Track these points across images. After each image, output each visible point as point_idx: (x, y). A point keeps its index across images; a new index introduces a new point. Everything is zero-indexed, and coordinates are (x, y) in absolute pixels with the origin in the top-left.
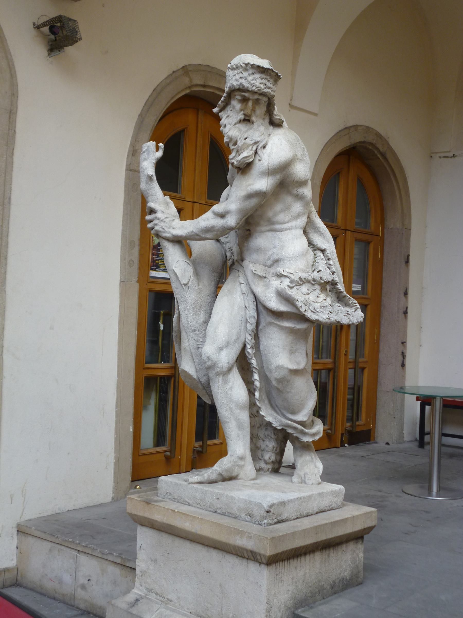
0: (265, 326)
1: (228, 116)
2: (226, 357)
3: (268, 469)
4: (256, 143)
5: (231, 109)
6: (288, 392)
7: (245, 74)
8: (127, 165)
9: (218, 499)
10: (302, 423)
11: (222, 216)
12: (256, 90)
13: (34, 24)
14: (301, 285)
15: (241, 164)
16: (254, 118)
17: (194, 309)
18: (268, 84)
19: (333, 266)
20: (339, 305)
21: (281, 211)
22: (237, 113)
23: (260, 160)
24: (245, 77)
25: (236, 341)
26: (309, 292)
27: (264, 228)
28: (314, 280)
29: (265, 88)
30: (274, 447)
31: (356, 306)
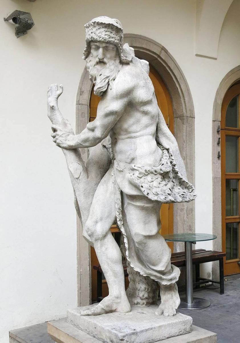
0: (127, 205)
1: (90, 61)
2: (102, 227)
3: (144, 303)
4: (108, 77)
5: (91, 56)
6: (147, 251)
7: (94, 30)
8: (77, 101)
9: (95, 328)
10: (162, 273)
11: (93, 130)
12: (103, 40)
13: (4, 19)
14: (147, 175)
15: (97, 93)
16: (105, 60)
17: (84, 195)
18: (112, 35)
19: (174, 160)
20: (179, 188)
21: (133, 124)
22: (95, 58)
23: (111, 89)
24: (94, 32)
25: (108, 217)
26: (153, 180)
27: (123, 137)
28: (156, 171)
29: (109, 38)
30: (145, 288)
31: (192, 188)
